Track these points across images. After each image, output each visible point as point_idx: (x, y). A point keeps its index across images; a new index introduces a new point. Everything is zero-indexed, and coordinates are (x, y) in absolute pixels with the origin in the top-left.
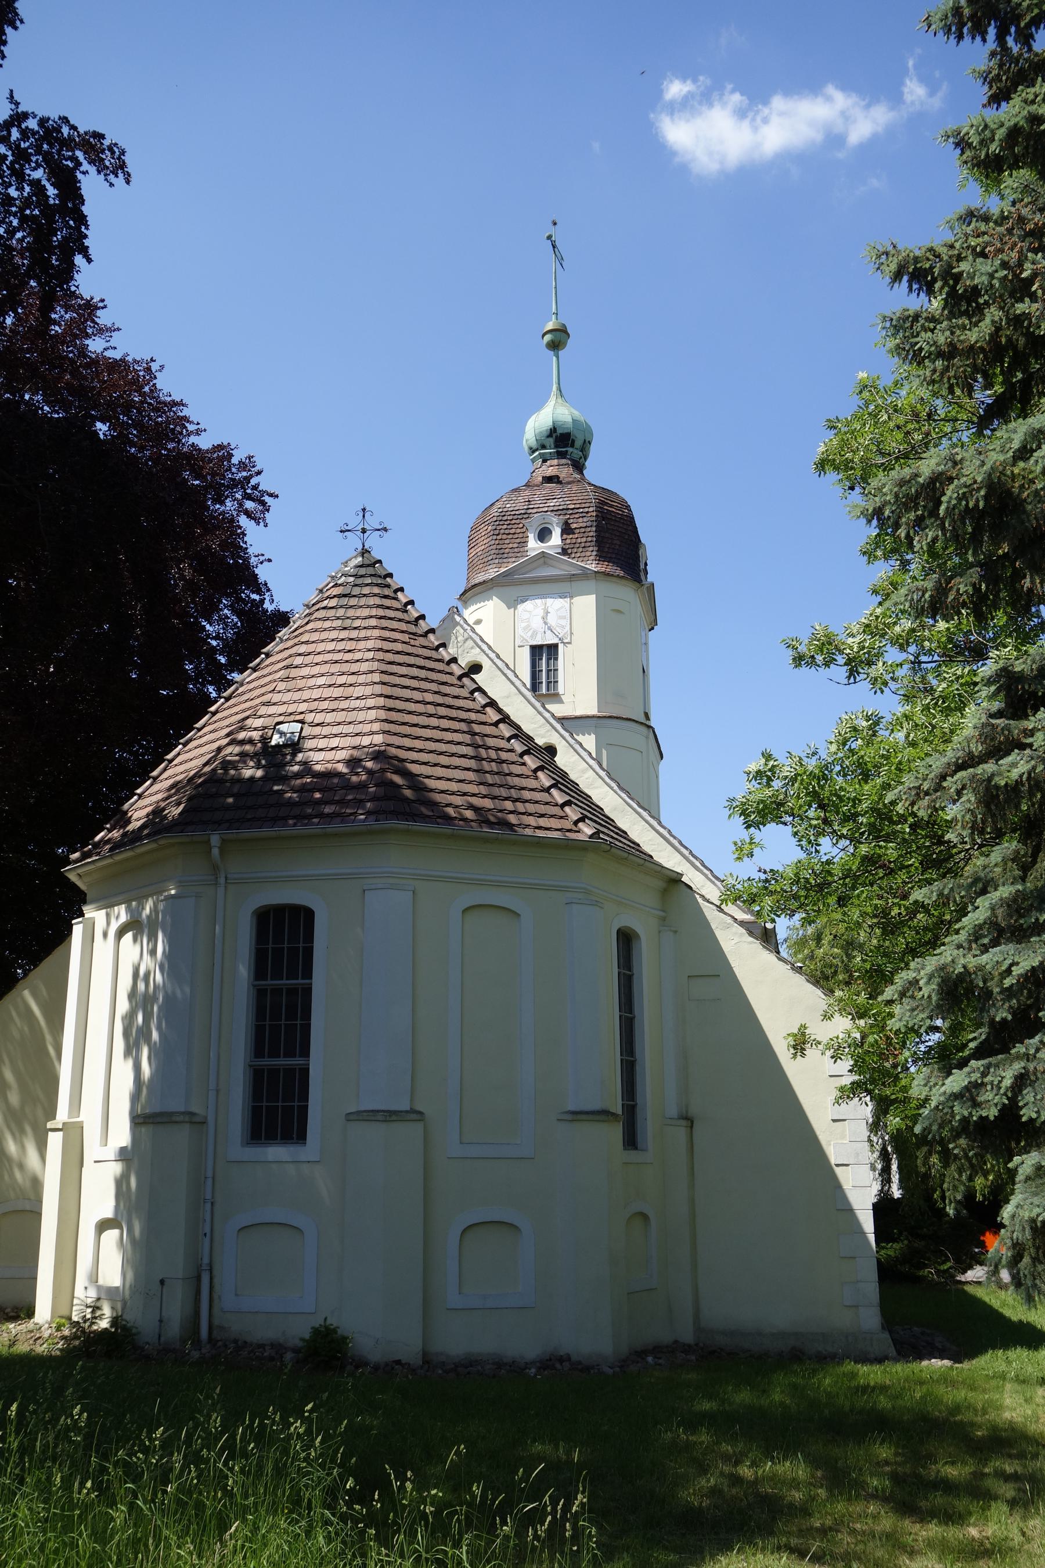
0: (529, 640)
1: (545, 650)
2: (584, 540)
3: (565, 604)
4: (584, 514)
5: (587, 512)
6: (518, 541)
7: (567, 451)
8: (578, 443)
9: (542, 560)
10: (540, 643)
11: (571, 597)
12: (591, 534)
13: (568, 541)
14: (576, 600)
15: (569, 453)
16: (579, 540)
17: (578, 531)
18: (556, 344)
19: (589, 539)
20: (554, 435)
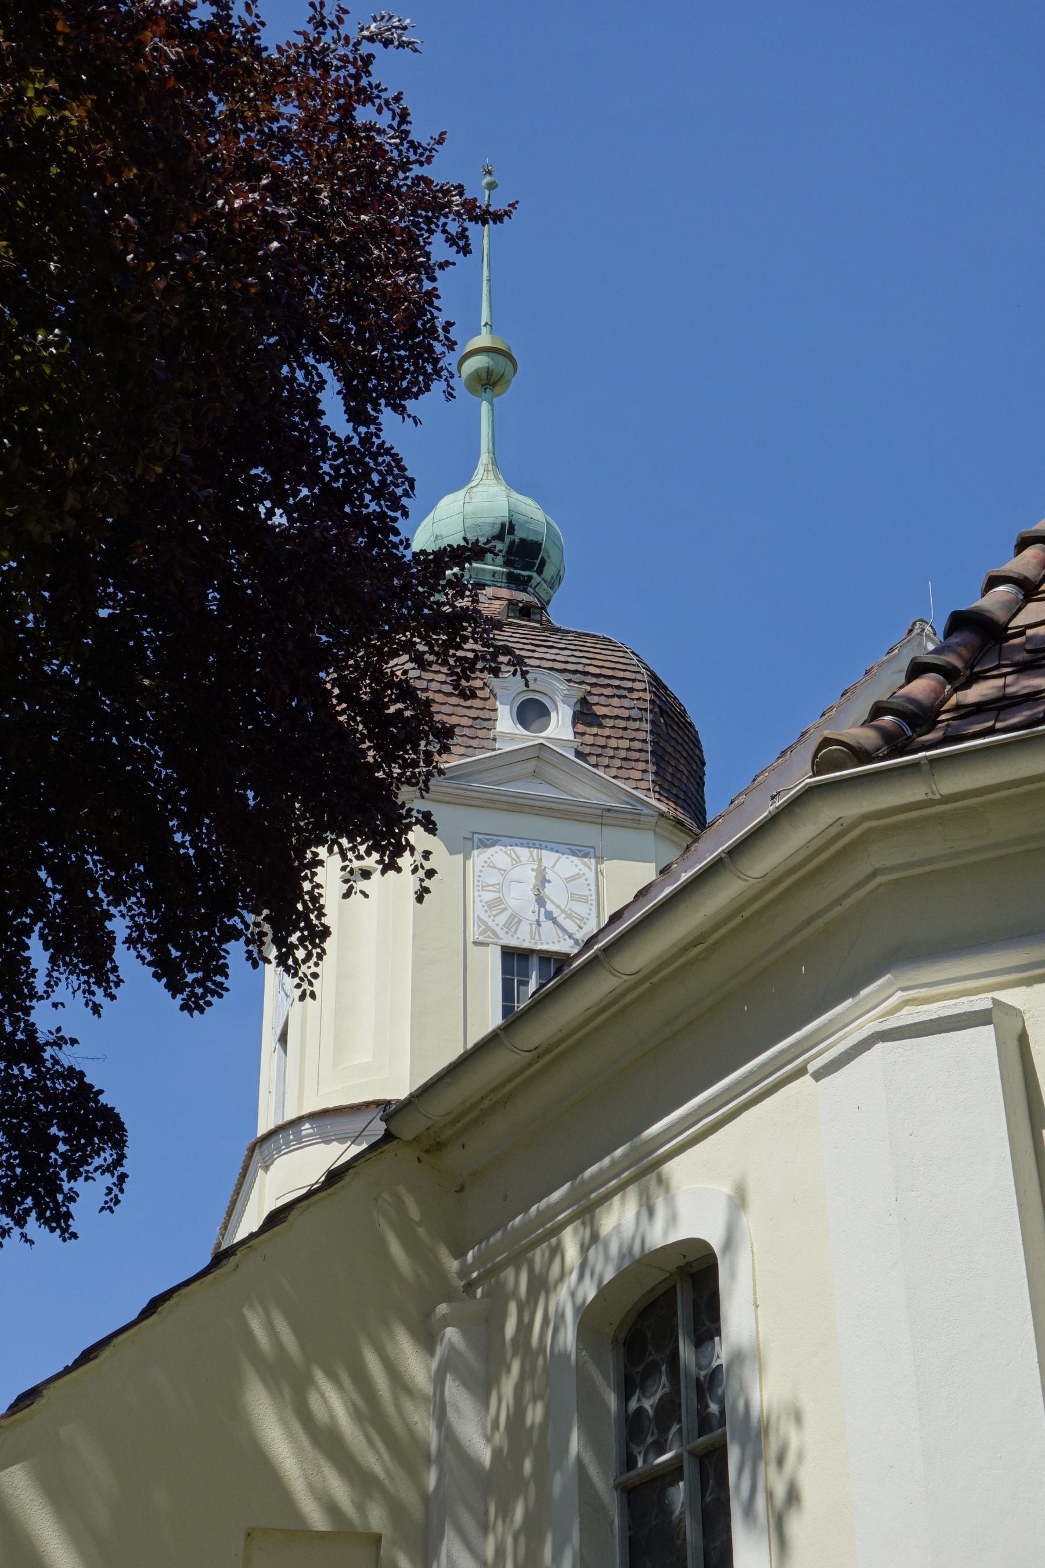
0: (501, 933)
1: (534, 962)
2: (626, 744)
3: (585, 870)
4: (625, 693)
5: (631, 690)
6: (473, 713)
7: (530, 578)
8: (549, 571)
9: (531, 766)
10: (526, 945)
11: (600, 859)
12: (641, 735)
13: (590, 740)
14: (607, 866)
15: (534, 583)
16: (613, 743)
17: (610, 722)
18: (494, 378)
19: (637, 745)
20: (508, 538)
